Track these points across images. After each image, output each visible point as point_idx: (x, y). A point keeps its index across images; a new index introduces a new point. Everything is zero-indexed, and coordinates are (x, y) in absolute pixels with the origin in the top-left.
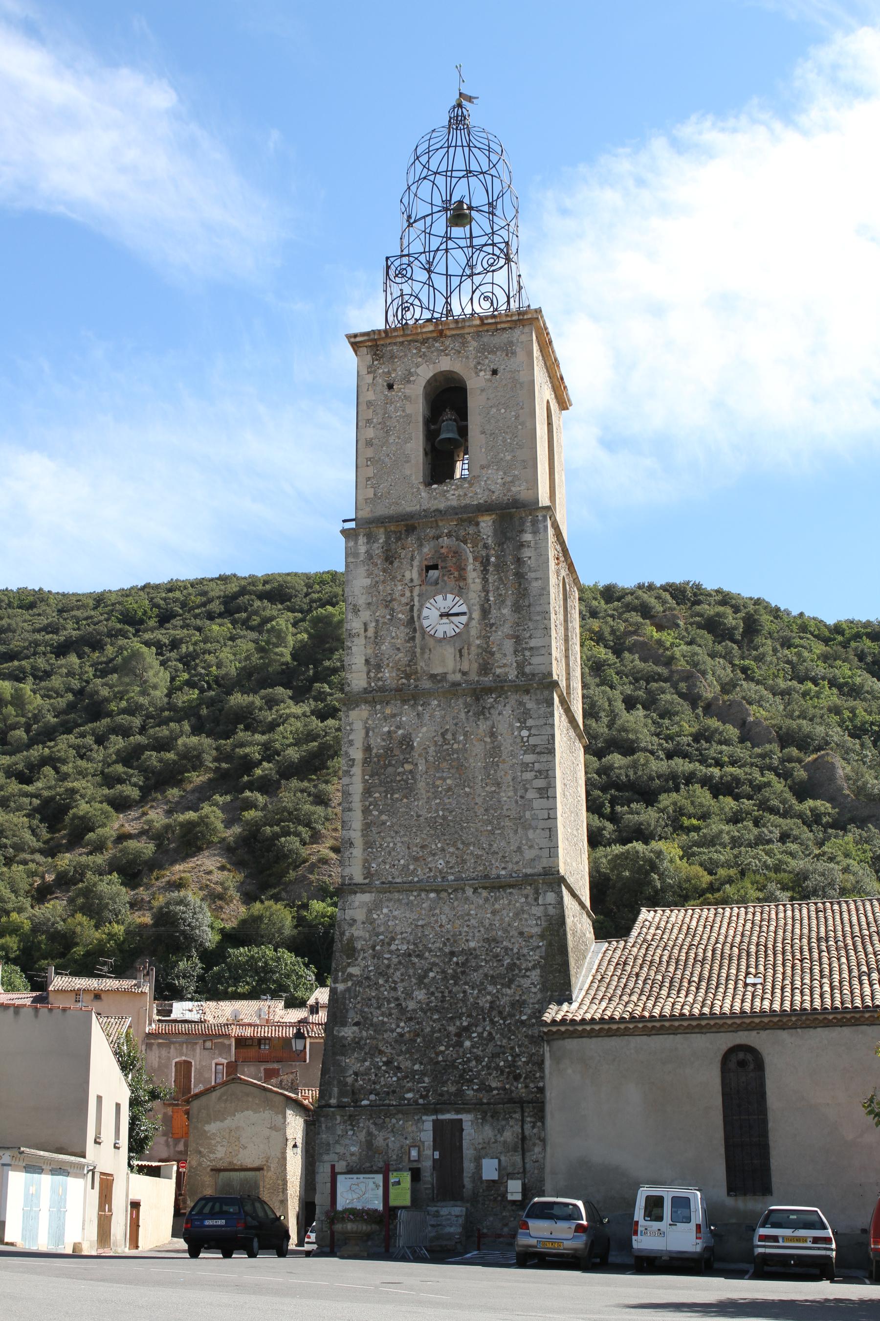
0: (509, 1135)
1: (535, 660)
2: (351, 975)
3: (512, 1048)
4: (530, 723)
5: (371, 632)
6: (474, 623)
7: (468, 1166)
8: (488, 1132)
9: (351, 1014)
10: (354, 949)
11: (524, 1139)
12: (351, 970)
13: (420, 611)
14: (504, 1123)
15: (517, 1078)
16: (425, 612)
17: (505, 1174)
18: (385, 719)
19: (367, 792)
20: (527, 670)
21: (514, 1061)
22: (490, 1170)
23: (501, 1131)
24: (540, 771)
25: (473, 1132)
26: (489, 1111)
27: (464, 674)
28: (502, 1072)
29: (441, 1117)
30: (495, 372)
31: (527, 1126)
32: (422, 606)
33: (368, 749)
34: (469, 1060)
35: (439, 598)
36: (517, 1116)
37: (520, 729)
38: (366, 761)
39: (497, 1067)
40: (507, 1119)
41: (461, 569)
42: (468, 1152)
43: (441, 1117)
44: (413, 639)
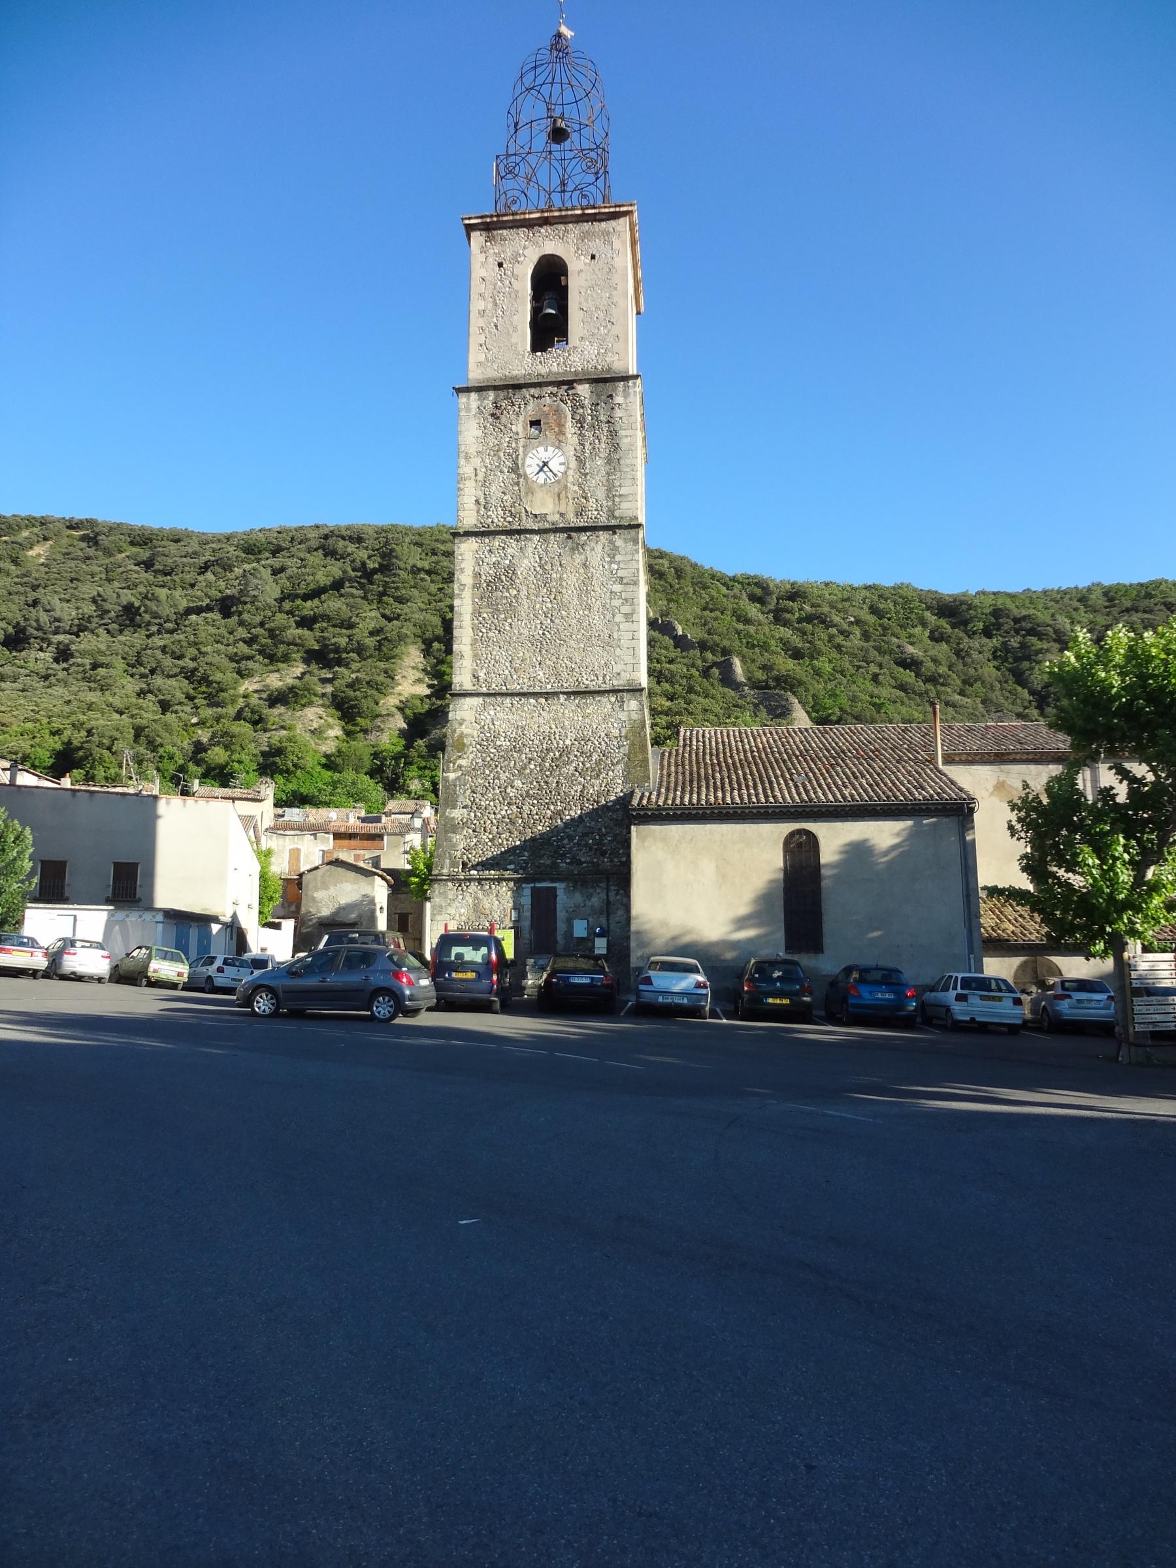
0: (596, 901)
1: (624, 505)
2: (460, 767)
3: (600, 829)
4: (618, 558)
5: (481, 477)
6: (571, 472)
7: (561, 926)
8: (578, 898)
9: (461, 798)
10: (464, 745)
11: (608, 903)
12: (460, 762)
13: (524, 459)
14: (591, 891)
15: (603, 854)
16: (528, 461)
17: (592, 935)
18: (386, 531)
19: (477, 613)
20: (617, 513)
21: (601, 840)
22: (580, 929)
23: (589, 897)
24: (626, 600)
25: (564, 898)
26: (578, 881)
27: (562, 515)
28: (591, 849)
29: (538, 885)
30: (593, 257)
31: (612, 894)
32: (525, 455)
33: (477, 575)
34: (563, 838)
35: (541, 449)
36: (603, 885)
37: (610, 563)
38: (476, 586)
39: (586, 845)
40: (593, 887)
41: (561, 425)
42: (561, 914)
43: (538, 885)
44: (518, 484)
